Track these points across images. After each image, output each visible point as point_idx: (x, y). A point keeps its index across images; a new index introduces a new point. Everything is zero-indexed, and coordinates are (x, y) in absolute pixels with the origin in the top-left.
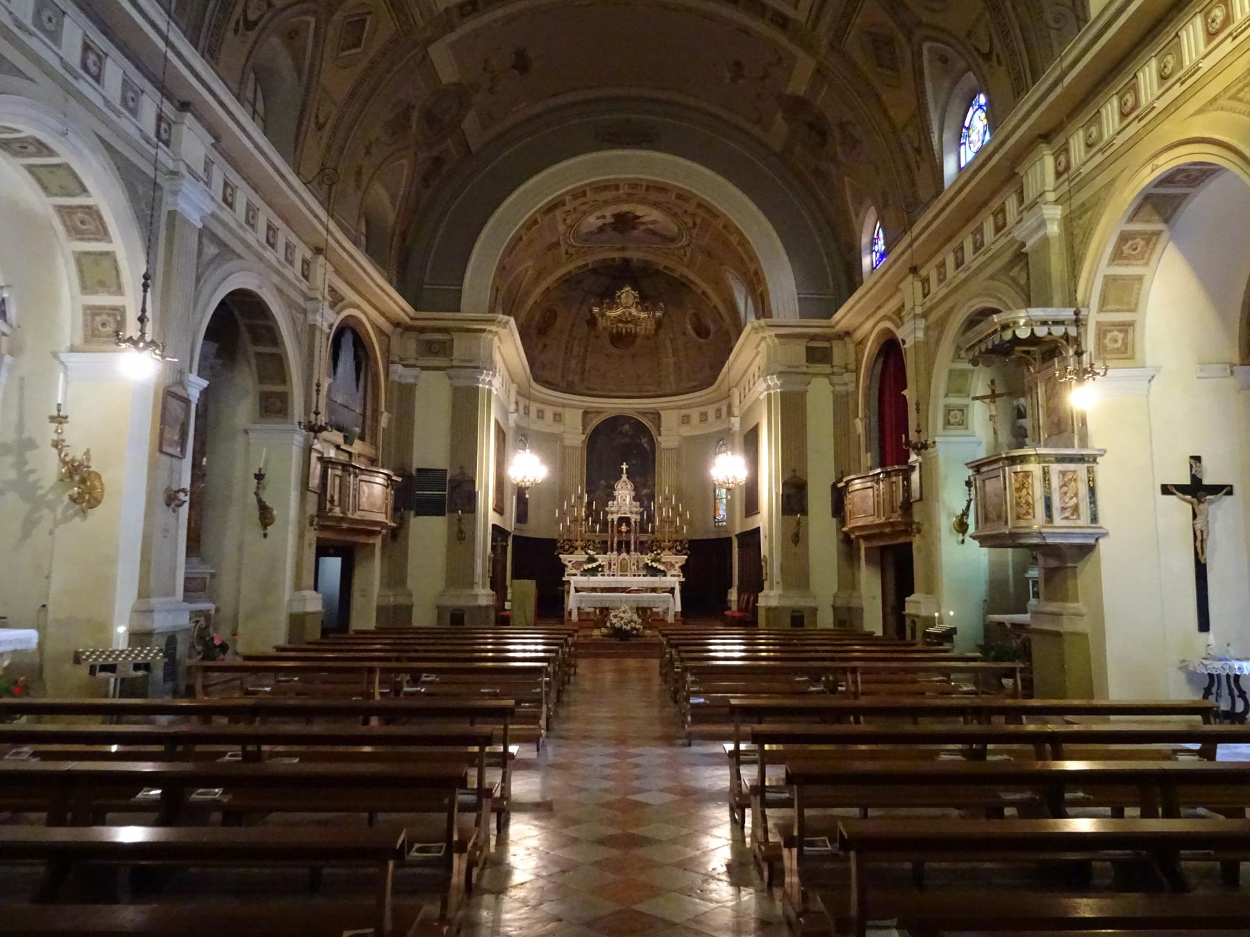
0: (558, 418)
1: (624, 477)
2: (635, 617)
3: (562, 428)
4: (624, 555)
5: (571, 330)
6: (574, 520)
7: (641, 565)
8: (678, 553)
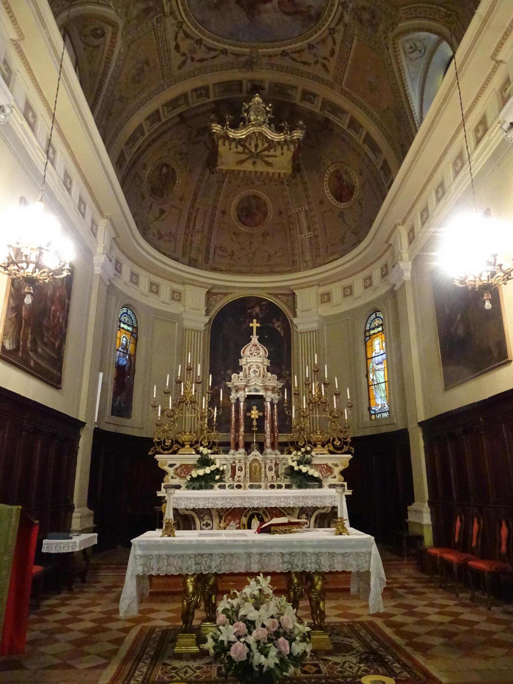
0: (177, 296)
1: (255, 339)
2: (289, 618)
3: (182, 309)
4: (255, 454)
5: (194, 200)
6: (180, 403)
7: (282, 470)
8: (336, 450)
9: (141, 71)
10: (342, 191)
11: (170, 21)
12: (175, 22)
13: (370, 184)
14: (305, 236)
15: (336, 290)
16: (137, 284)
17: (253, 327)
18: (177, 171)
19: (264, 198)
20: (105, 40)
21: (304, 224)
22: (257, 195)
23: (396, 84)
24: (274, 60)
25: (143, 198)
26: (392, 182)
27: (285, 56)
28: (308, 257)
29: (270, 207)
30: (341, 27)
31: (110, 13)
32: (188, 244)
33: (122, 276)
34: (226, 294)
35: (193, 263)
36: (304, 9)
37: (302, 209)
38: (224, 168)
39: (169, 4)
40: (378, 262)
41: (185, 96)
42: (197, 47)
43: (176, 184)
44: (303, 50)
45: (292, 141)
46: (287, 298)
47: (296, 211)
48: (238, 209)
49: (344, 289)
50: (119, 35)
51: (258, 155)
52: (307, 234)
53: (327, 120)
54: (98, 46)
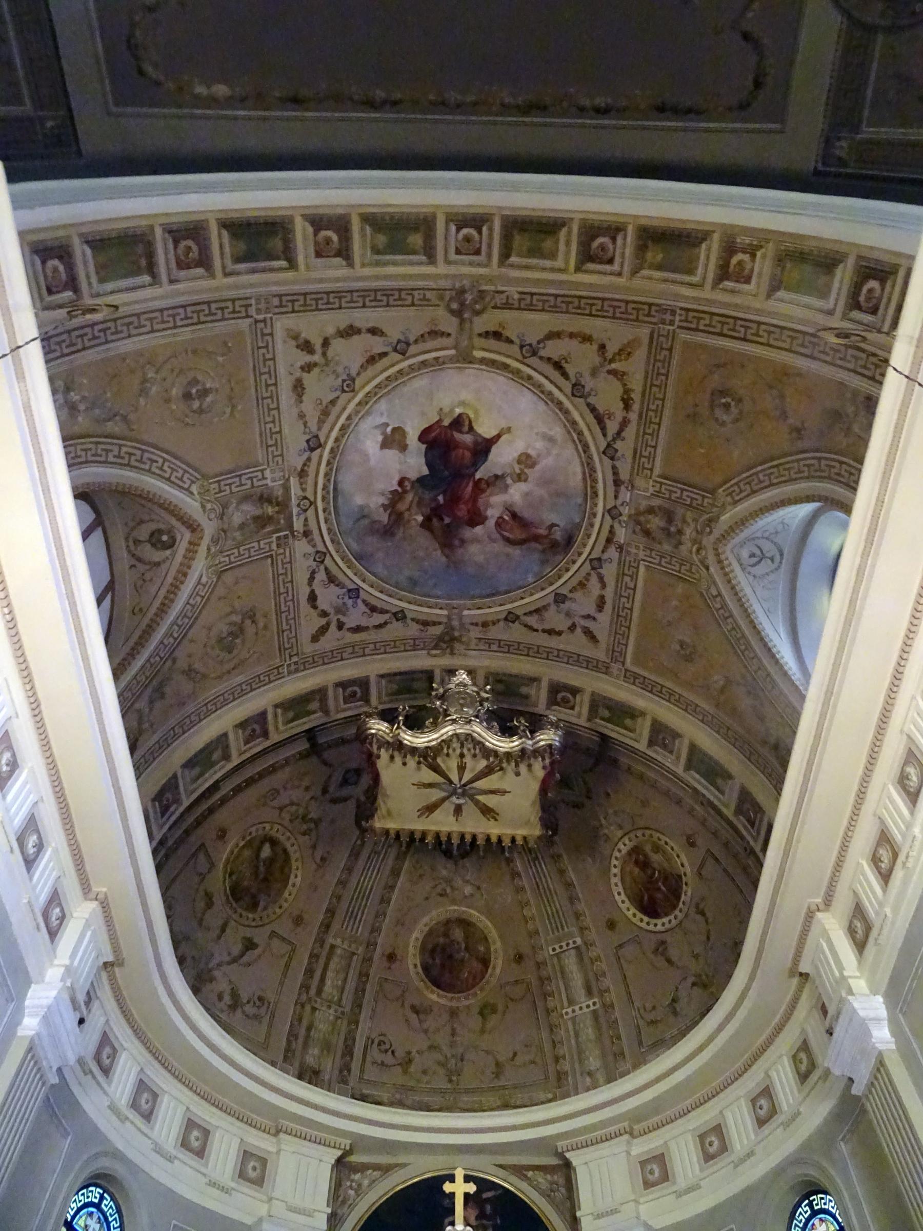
0: (253, 1170)
3: (263, 1210)
5: (326, 927)
9: (238, 631)
10: (656, 893)
11: (301, 547)
12: (310, 550)
13: (716, 859)
14: (581, 1008)
15: (680, 1144)
16: (148, 1116)
17: (453, 1195)
18: (294, 857)
19: (480, 925)
20: (174, 555)
21: (577, 980)
22: (464, 917)
23: (736, 627)
24: (495, 633)
25: (210, 904)
26: (770, 827)
27: (513, 622)
28: (594, 1062)
29: (497, 946)
30: (612, 553)
31: (191, 505)
32: (302, 1032)
33: (109, 1084)
34: (386, 1169)
35: (309, 1075)
36: (542, 532)
37: (568, 945)
38: (392, 825)
39: (302, 518)
40: (779, 1040)
41: (320, 693)
42: (350, 602)
43: (290, 886)
44: (545, 608)
45: (537, 753)
46: (549, 1177)
47: (554, 950)
48: (423, 948)
49: (702, 1137)
50: (202, 550)
51: (466, 791)
52: (585, 1005)
53: (604, 738)
54: (158, 564)
